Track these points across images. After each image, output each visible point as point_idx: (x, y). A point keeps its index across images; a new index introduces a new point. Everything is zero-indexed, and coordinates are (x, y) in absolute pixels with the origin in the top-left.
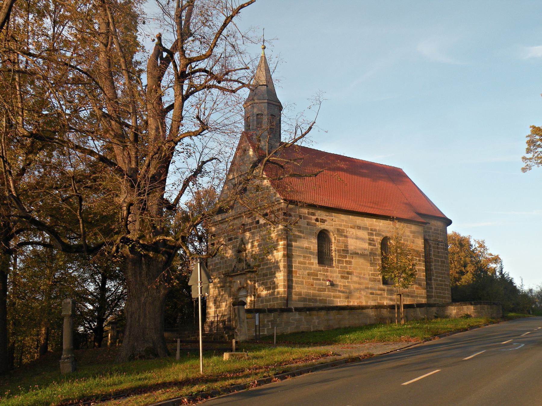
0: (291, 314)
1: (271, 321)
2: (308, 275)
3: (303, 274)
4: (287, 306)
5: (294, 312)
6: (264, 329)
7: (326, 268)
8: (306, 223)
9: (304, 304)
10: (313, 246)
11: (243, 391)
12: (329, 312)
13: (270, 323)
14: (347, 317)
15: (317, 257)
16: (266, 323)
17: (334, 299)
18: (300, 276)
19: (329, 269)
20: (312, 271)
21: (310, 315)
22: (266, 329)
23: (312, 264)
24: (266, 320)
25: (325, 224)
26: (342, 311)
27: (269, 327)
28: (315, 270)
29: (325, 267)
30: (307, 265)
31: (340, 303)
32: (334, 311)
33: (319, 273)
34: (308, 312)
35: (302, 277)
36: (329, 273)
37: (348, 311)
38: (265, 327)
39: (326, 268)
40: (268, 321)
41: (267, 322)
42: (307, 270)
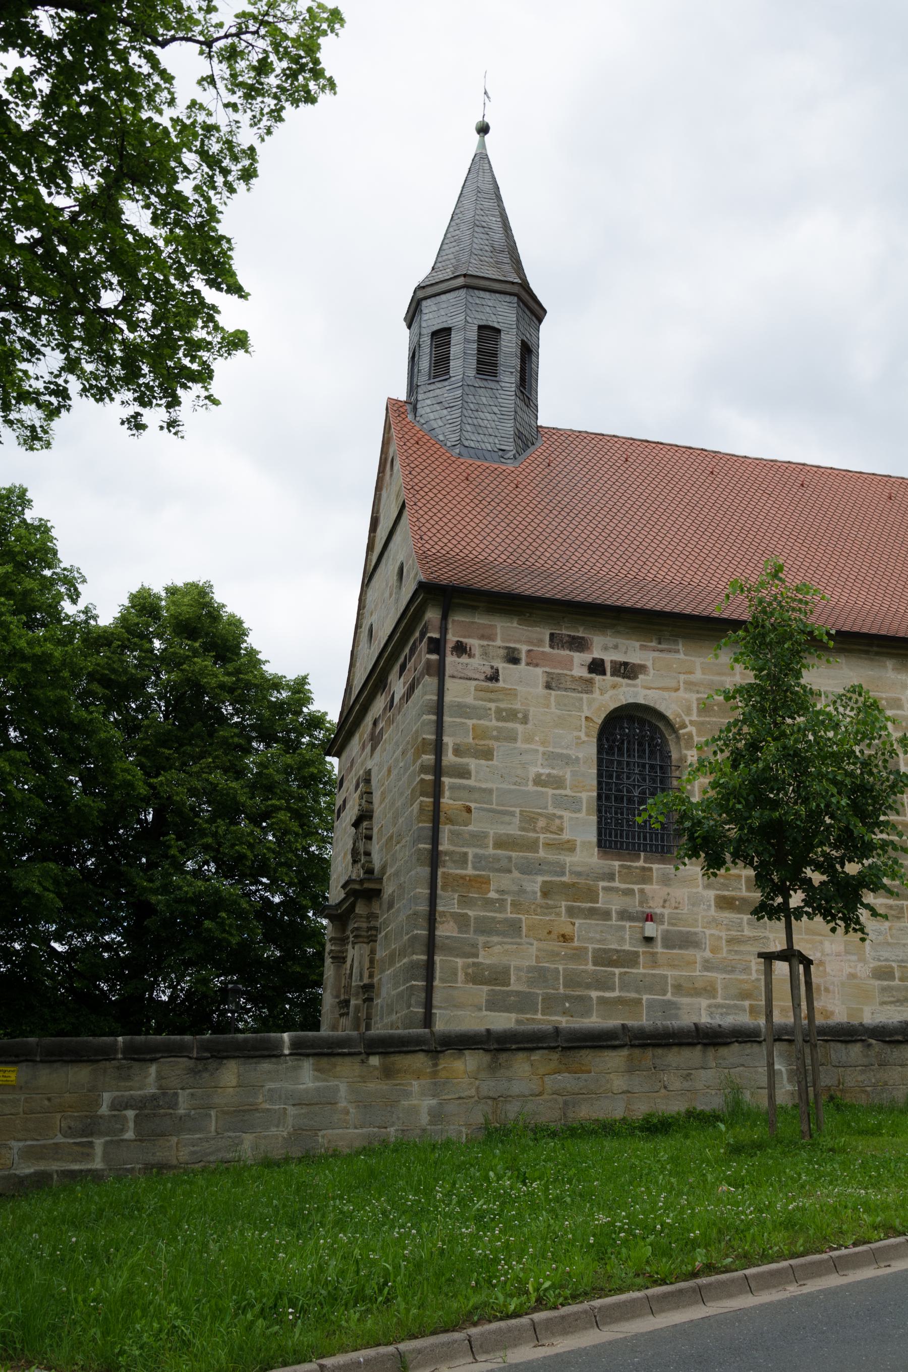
0: (266, 1066)
1: (141, 1104)
2: (545, 894)
3: (522, 891)
4: (428, 1020)
5: (290, 1062)
6: (90, 1144)
7: (641, 863)
8: (541, 680)
9: (518, 1022)
10: (574, 774)
11: (371, 1352)
12: (503, 1057)
13: (130, 1114)
14: (619, 1083)
15: (594, 818)
16: (104, 1110)
17: (685, 1000)
18: (503, 901)
19: (655, 866)
20: (565, 879)
21: (388, 1073)
22: (99, 1143)
23: (570, 847)
24: (107, 1097)
25: (638, 681)
26: (587, 1057)
27: (122, 1131)
28: (579, 874)
29: (638, 858)
30: (542, 853)
31: (711, 1015)
32: (536, 1056)
33: (602, 884)
34: (375, 1061)
35: (513, 904)
36: (655, 887)
37: (625, 1052)
38: (101, 1134)
39: (641, 863)
40: (118, 1106)
41: (113, 1107)
42: (540, 872)
